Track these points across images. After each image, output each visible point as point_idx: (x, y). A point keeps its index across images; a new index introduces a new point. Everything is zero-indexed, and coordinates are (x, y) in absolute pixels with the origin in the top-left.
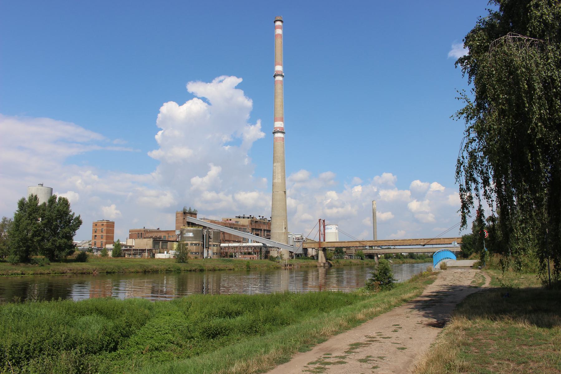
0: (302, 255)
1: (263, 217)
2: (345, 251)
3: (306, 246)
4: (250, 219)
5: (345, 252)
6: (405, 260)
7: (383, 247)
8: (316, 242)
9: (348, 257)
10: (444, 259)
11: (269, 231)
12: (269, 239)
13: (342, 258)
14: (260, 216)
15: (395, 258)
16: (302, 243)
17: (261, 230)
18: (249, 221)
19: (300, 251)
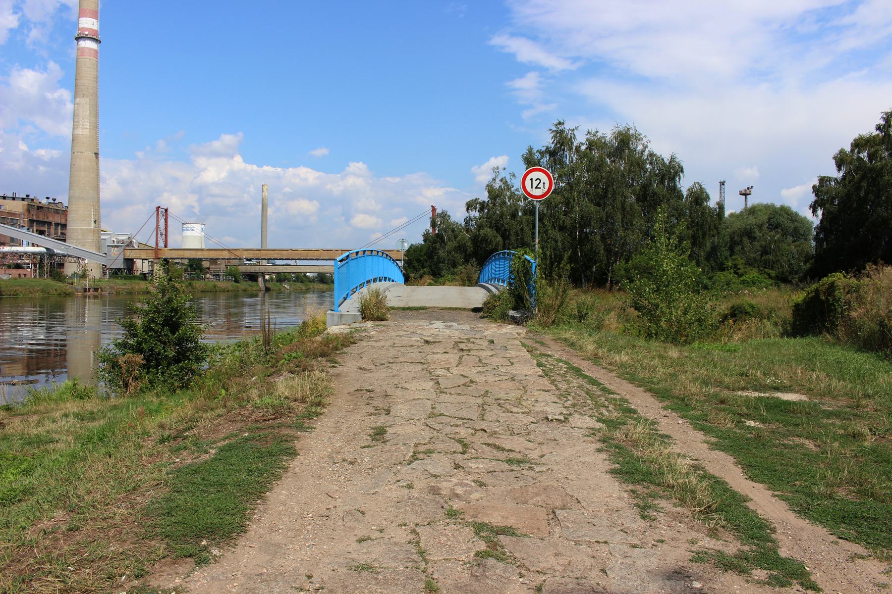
1: (54, 200)
3: (130, 254)
4: (26, 203)
5: (208, 269)
6: (311, 285)
7: (277, 262)
9: (211, 277)
10: (375, 280)
11: (64, 226)
12: (64, 240)
14: (48, 198)
15: (294, 281)
16: (122, 248)
17: (50, 224)
18: (24, 205)
19: (120, 264)
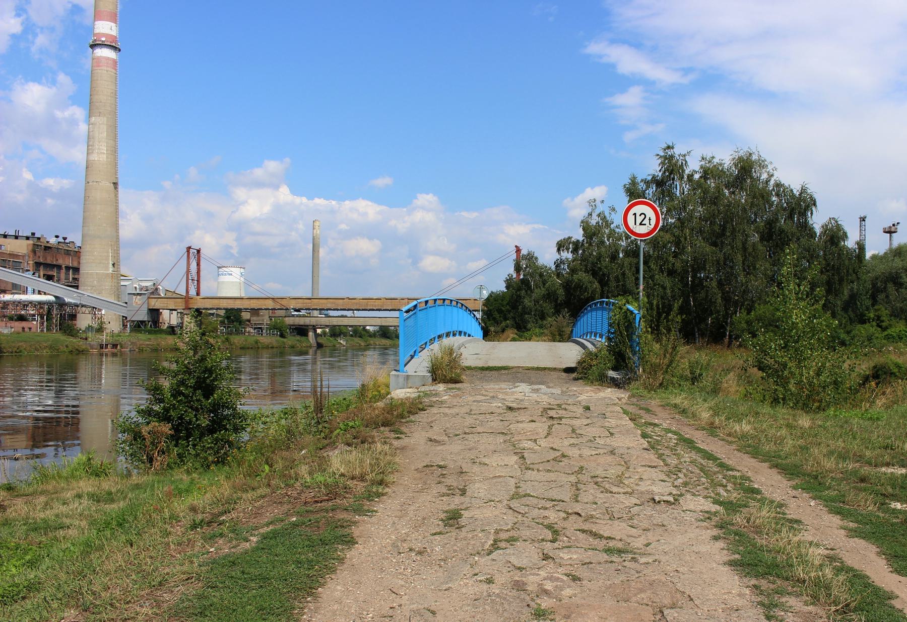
0: (145, 324)
1: (65, 239)
2: (248, 318)
3: (155, 304)
4: (30, 242)
5: (249, 321)
6: (371, 341)
7: (331, 313)
8: (181, 297)
10: (448, 335)
11: (76, 270)
12: (77, 287)
13: (238, 332)
14: (57, 237)
15: (352, 336)
16: (146, 296)
17: (59, 267)
18: (28, 245)
19: (143, 316)
